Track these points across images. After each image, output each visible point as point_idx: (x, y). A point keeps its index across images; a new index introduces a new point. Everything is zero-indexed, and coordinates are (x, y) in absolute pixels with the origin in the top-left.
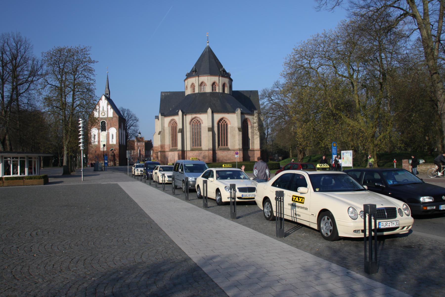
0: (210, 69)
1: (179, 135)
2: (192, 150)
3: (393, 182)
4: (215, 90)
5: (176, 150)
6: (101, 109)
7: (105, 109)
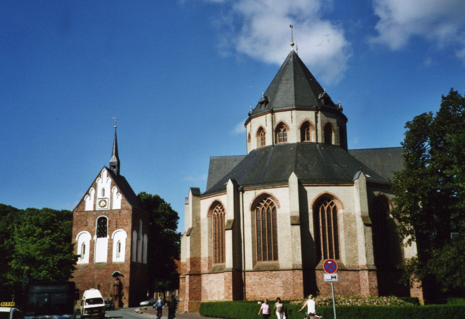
0: (295, 95)
1: (229, 235)
2: (257, 270)
3: (101, 274)
4: (308, 138)
5: (221, 270)
6: (99, 195)
7: (107, 195)
